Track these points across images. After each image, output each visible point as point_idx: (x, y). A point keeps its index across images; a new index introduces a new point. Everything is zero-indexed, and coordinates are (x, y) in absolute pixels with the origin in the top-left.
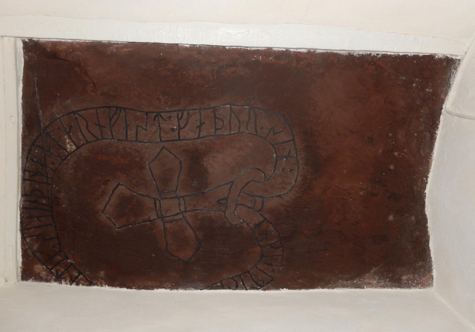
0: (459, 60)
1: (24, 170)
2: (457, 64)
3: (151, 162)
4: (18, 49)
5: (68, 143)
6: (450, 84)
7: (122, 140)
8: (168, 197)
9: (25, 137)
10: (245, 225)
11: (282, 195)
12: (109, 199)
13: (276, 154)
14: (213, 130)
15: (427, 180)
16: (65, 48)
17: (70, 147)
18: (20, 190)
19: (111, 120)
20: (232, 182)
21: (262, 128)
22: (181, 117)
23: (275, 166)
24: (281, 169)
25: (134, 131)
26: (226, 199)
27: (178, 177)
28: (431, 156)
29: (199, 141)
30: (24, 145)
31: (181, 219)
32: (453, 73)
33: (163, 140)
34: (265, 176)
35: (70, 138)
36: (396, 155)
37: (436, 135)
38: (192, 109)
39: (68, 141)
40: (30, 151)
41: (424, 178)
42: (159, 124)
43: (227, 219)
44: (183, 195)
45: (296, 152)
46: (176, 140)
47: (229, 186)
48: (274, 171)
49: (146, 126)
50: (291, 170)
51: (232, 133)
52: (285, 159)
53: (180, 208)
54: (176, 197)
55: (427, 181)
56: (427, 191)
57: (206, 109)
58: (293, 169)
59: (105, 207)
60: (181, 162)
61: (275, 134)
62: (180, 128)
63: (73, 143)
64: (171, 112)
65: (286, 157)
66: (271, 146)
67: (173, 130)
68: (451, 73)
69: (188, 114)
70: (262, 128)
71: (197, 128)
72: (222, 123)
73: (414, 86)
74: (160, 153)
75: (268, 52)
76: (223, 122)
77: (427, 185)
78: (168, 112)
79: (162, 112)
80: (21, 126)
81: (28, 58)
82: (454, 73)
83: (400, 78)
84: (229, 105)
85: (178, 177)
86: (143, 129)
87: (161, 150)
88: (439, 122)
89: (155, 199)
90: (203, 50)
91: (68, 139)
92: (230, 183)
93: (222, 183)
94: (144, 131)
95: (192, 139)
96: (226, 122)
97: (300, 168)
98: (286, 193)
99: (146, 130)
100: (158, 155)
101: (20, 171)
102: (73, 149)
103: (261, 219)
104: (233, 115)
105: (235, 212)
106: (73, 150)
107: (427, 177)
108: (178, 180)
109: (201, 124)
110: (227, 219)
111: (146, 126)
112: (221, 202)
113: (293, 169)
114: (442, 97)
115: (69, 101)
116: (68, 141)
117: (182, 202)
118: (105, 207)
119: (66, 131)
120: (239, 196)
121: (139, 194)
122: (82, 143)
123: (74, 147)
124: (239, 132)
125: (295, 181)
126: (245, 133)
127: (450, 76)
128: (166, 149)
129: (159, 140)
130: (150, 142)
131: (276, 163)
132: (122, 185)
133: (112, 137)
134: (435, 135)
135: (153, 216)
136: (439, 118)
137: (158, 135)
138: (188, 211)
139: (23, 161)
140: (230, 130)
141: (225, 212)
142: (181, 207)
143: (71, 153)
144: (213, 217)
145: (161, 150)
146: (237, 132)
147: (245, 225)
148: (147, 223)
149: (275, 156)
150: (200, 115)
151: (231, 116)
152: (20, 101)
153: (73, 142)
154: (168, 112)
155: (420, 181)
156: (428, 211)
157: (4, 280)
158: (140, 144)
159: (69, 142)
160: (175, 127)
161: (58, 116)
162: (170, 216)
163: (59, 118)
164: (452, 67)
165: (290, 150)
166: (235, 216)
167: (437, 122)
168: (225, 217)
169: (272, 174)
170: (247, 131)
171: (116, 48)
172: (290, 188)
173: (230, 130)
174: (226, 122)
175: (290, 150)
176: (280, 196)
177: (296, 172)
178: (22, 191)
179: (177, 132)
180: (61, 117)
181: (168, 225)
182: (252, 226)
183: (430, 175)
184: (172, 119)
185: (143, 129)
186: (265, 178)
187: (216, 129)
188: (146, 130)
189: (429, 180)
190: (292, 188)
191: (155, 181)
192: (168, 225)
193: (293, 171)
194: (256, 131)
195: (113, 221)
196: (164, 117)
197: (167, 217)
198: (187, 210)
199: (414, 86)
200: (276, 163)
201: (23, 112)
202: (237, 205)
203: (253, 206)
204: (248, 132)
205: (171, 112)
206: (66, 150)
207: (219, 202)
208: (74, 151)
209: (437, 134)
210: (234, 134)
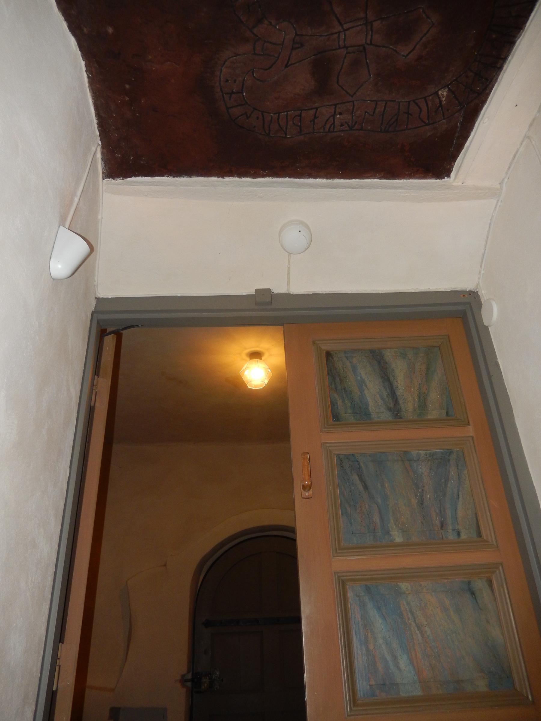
0: (103, 179)
1: (500, 68)
2: (104, 176)
3: (367, 81)
4: (455, 173)
5: (444, 96)
6: (103, 161)
7: (391, 101)
8: (356, 48)
9: (484, 102)
10: (273, 22)
11: (234, 56)
12: (421, 39)
13: (243, 95)
14: (303, 115)
15: (87, 74)
16: (417, 176)
17: (443, 93)
18: (513, 51)
19: (397, 120)
20: (286, 66)
21: (258, 118)
22: (331, 125)
23: (243, 84)
24: (237, 82)
25: (377, 111)
26: (293, 49)
27: (342, 68)
28: (93, 99)
29: (317, 105)
30: (489, 94)
31: (345, 23)
32: (104, 169)
33: (351, 103)
34: (253, 74)
35: (441, 102)
36: (127, 98)
37: (97, 118)
38: (321, 133)
39: (444, 99)
40: (485, 89)
41: (91, 76)
42: (352, 119)
43: (294, 27)
44: (339, 50)
45: (223, 97)
46: (338, 104)
47: (290, 63)
48: (244, 80)
49: (365, 115)
50: (227, 81)
51: (285, 113)
52: (234, 91)
53: (345, 36)
54: (346, 47)
55: (87, 73)
56: (83, 63)
57: (309, 133)
58: (226, 81)
59: (428, 31)
60: (338, 82)
61: (246, 114)
62: (334, 115)
63: (440, 96)
64: (339, 131)
65: (233, 92)
66: (248, 103)
67: (340, 114)
68: (106, 169)
69: (324, 129)
70: (258, 118)
71: (318, 117)
72: (295, 122)
73: (131, 157)
74: (357, 91)
75: (255, 175)
76: (293, 122)
77: (86, 69)
78: (343, 131)
79: (347, 130)
80: (482, 112)
81: (451, 163)
82: (103, 170)
83: (145, 162)
84: (288, 137)
85: (342, 68)
86: (368, 113)
87: (355, 93)
88: (98, 130)
89: (371, 44)
90: (307, 176)
91: (443, 100)
92: (289, 66)
93: (297, 64)
94: (368, 111)
95: (324, 106)
96: (291, 123)
97: (218, 84)
98: (231, 58)
99: (366, 112)
100: (359, 88)
101: (505, 68)
102: (441, 91)
103: (255, 31)
104: (284, 129)
105: (285, 36)
106: (442, 90)
107: (88, 77)
108: (343, 65)
109: (313, 120)
110: (294, 27)
111: (365, 115)
112: (299, 45)
113: (226, 81)
114: (105, 151)
115: (429, 134)
116: (444, 99)
117: (341, 43)
118: (428, 31)
119: (442, 109)
120: (280, 54)
121: (386, 47)
122: (431, 98)
123: (440, 92)
124: (279, 113)
125: (221, 70)
126: (274, 113)
127: (105, 167)
128: (350, 95)
129: (355, 103)
130: (364, 100)
131: (243, 87)
132: (403, 56)
133: (399, 104)
134: (97, 118)
135: (377, 24)
136: (99, 132)
137: (355, 108)
138: (336, 33)
139: (497, 79)
140: (287, 116)
141: (297, 35)
142: (344, 37)
143: (445, 87)
144: (309, 28)
145: (355, 93)
146: (281, 114)
147: (273, 22)
148: (385, 16)
149: (244, 94)
150: (314, 128)
151: (286, 129)
152: (472, 134)
153: (439, 98)
154: (343, 131)
155: (94, 73)
156: (72, 41)
157: (516, 105)
158: (375, 99)
159: (443, 98)
160: (338, 116)
161: (444, 121)
162: (358, 26)
163: (444, 119)
164: (107, 174)
165: (230, 100)
166: (284, 32)
167: (100, 128)
168: (295, 29)
169: (245, 76)
170: (271, 115)
171: (376, 176)
172: (227, 63)
173: (287, 116)
174: (291, 123)
175: (230, 100)
176: (236, 55)
177: (222, 79)
178: (513, 47)
179: (337, 113)
180: (442, 120)
181: (362, 15)
182: (266, 22)
183: (86, 80)
184: (340, 124)
185: (368, 113)
186: (253, 72)
187: (300, 115)
188: (366, 112)
189: (85, 75)
190: (224, 64)
191: (367, 62)
192: (362, 15)
193: (225, 80)
194: (262, 115)
195: (424, 15)
196: (346, 125)
197: (361, 25)
198: (337, 35)
199: (131, 157)
200: (243, 87)
201: (474, 124)
202: (282, 44)
203: (265, 45)
204: (270, 114)
205: (339, 131)
206: (450, 90)
207: (302, 45)
208: (439, 90)
209: (96, 119)
210: (284, 112)
